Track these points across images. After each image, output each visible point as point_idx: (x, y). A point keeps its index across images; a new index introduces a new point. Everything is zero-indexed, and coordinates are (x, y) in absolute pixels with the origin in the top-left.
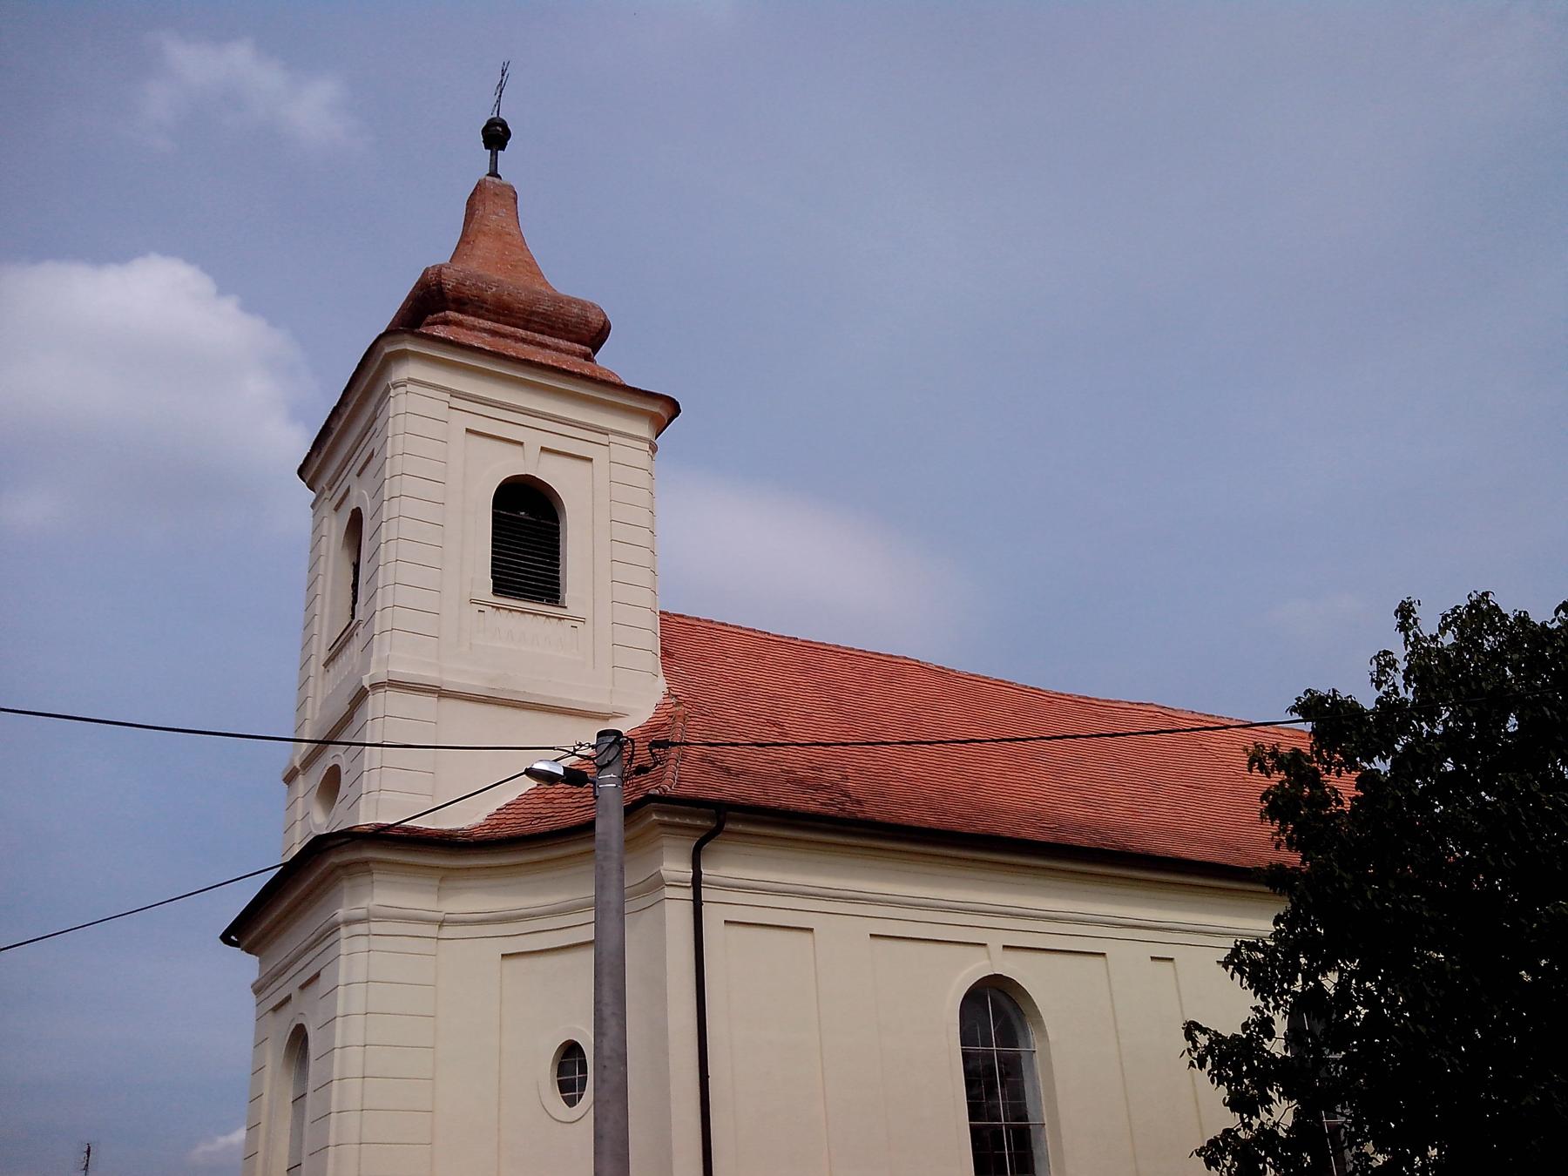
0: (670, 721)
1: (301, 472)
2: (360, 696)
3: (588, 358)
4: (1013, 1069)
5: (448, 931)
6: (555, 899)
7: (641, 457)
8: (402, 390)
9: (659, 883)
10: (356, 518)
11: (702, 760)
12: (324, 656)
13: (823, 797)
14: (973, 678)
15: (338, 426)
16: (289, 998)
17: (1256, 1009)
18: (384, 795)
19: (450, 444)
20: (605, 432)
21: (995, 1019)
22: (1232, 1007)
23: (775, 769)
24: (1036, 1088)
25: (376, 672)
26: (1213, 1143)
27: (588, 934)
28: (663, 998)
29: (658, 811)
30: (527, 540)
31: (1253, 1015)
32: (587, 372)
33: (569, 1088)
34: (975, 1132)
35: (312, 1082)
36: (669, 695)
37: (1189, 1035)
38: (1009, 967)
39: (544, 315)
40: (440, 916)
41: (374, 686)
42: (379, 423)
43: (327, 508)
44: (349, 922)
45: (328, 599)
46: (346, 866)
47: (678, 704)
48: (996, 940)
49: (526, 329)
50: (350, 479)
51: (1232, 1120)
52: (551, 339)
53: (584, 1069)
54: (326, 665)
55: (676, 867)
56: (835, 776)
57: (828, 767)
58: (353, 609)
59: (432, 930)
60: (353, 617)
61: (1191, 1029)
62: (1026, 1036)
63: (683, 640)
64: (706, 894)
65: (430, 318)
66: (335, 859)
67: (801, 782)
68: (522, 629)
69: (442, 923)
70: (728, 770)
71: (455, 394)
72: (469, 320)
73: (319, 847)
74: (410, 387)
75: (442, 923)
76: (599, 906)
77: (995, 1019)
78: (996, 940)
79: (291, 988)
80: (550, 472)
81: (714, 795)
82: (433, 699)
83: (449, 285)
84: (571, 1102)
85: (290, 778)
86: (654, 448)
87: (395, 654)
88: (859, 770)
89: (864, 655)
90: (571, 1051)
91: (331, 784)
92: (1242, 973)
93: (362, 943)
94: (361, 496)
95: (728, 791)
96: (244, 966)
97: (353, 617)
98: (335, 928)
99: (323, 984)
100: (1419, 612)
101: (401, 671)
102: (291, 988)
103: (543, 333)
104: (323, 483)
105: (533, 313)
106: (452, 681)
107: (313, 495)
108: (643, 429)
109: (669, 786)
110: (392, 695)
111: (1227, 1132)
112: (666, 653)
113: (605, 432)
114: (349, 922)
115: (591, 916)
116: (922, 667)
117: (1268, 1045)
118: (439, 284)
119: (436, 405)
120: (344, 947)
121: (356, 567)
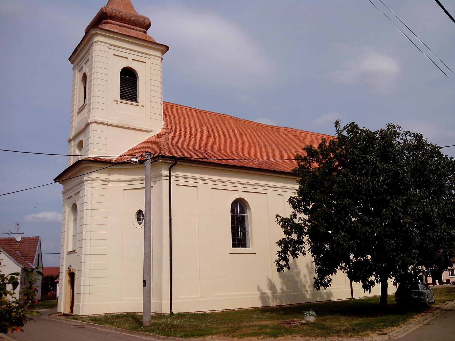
0: (165, 133)
1: (69, 59)
2: (88, 125)
3: (145, 33)
4: (243, 219)
5: (111, 183)
6: (135, 178)
7: (158, 62)
8: (96, 43)
9: (161, 176)
10: (85, 76)
11: (173, 145)
12: (77, 111)
13: (201, 156)
14: (244, 121)
15: (79, 49)
16: (72, 196)
17: (293, 212)
18: (94, 150)
19: (109, 58)
20: (149, 55)
21: (239, 210)
22: (287, 211)
23: (191, 147)
24: (248, 224)
25: (91, 119)
26: (280, 241)
27: (144, 186)
28: (161, 202)
29: (161, 159)
30: (129, 83)
31: (292, 213)
32: (144, 38)
33: (139, 220)
34: (233, 233)
35: (78, 217)
36: (165, 126)
37: (276, 217)
38: (244, 196)
39: (133, 21)
40: (109, 180)
41: (91, 123)
42: (91, 51)
43: (76, 71)
44: (86, 181)
45: (78, 95)
46: (86, 167)
47: (167, 129)
48: (241, 190)
49: (129, 24)
50: (83, 64)
51: (285, 236)
52: (136, 28)
53: (143, 216)
54: (78, 113)
55: (165, 172)
56: (205, 149)
57: (204, 147)
58: (85, 101)
59: (107, 183)
60: (85, 102)
61: (277, 216)
62: (247, 211)
63: (169, 110)
64: (172, 178)
65: (103, 21)
66: (83, 166)
67: (197, 151)
68: (127, 107)
69: (109, 181)
70: (178, 148)
71: (110, 45)
72: (114, 22)
73: (78, 163)
74: (99, 43)
75: (109, 181)
76: (146, 179)
77: (239, 210)
78: (241, 190)
79: (72, 194)
80: (135, 66)
81: (175, 155)
82: (106, 126)
83: (108, 13)
84: (140, 223)
85: (70, 141)
86: (162, 59)
87: (96, 116)
88: (212, 148)
89: (217, 114)
90: (140, 212)
91: (80, 145)
92: (291, 203)
93: (90, 185)
94: (86, 69)
95: (178, 154)
96: (59, 187)
97: (85, 102)
98: (83, 182)
99: (81, 194)
100: (340, 123)
101: (98, 119)
102: (72, 194)
103: (133, 25)
104: (76, 63)
105: (130, 20)
106: (110, 122)
107: (72, 66)
108: (159, 54)
109: (164, 153)
110: (96, 125)
111: (283, 239)
112: (164, 114)
113: (149, 55)
114: (86, 181)
115: (144, 182)
116: (231, 118)
117: (294, 220)
118: (106, 12)
119: (105, 48)
120: (86, 186)
121: (85, 88)
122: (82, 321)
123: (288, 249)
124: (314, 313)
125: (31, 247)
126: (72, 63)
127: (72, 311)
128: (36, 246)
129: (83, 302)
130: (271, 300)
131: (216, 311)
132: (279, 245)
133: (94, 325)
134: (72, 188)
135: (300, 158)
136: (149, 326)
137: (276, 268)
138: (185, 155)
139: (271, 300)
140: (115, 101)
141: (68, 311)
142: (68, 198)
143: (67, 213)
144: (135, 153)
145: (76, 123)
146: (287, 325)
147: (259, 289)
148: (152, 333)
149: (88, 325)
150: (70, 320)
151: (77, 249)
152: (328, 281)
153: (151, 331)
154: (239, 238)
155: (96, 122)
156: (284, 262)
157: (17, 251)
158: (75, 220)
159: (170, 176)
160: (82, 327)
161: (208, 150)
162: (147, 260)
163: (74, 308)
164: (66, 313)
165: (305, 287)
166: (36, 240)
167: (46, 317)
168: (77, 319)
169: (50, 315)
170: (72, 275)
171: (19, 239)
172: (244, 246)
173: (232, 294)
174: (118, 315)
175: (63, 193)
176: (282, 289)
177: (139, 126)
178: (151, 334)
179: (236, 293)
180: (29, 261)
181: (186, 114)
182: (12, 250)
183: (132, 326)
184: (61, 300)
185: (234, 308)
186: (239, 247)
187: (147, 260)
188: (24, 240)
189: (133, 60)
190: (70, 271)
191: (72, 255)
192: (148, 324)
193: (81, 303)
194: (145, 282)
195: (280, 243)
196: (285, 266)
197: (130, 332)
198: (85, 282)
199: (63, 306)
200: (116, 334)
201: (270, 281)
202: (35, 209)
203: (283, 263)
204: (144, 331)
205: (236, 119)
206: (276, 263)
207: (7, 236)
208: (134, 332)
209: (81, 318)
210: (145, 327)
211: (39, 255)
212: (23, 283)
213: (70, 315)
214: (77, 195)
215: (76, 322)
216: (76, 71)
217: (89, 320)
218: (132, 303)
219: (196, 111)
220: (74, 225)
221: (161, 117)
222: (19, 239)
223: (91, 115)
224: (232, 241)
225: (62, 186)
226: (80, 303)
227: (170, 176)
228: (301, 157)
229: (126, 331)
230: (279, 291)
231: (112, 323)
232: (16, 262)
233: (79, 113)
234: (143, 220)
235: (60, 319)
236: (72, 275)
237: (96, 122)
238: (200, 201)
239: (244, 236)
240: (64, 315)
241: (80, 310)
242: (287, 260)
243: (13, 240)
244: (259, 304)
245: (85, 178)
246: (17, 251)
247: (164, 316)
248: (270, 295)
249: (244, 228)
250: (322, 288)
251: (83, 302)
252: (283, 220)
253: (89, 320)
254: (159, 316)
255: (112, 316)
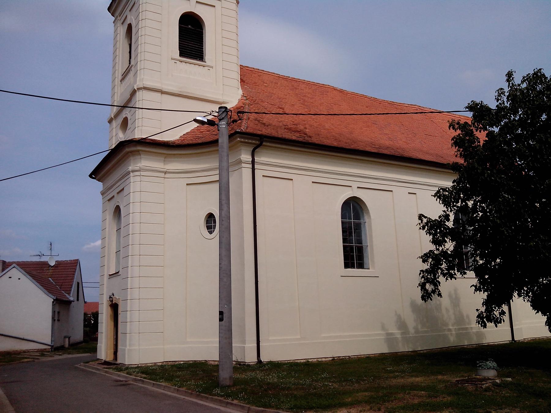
0: (243, 106)
4: (358, 228)
5: (167, 175)
6: (205, 166)
9: (240, 162)
10: (130, 27)
11: (255, 120)
12: (120, 77)
14: (353, 94)
16: (113, 197)
17: (444, 211)
18: (143, 128)
21: (353, 211)
22: (436, 210)
23: (281, 124)
24: (366, 234)
29: (240, 137)
31: (443, 213)
34: (344, 247)
38: (359, 194)
40: (165, 170)
41: (139, 89)
43: (119, 23)
44: (133, 171)
46: (131, 152)
47: (246, 100)
48: (355, 185)
51: (433, 247)
53: (215, 222)
55: (246, 157)
58: (130, 61)
59: (162, 175)
60: (130, 63)
61: (421, 217)
62: (363, 217)
63: (248, 76)
64: (256, 166)
66: (127, 150)
67: (290, 129)
68: (189, 69)
69: (165, 173)
70: (264, 124)
73: (122, 145)
75: (165, 173)
76: (220, 169)
77: (353, 211)
78: (355, 185)
79: (114, 193)
80: (200, 11)
81: (259, 133)
82: (159, 94)
84: (211, 233)
85: (110, 121)
87: (145, 78)
88: (311, 126)
91: (125, 124)
93: (138, 178)
94: (131, 19)
95: (265, 131)
96: (98, 186)
97: (130, 63)
98: (129, 173)
99: (125, 192)
100: (515, 75)
101: (149, 83)
102: (114, 193)
104: (117, 14)
106: (166, 88)
107: (113, 18)
110: (145, 92)
112: (242, 81)
114: (133, 171)
115: (217, 172)
116: (335, 89)
120: (132, 179)
122: (127, 374)
123: (437, 267)
124: (494, 364)
125: (68, 273)
126: (113, 15)
127: (116, 358)
128: (75, 272)
129: (130, 345)
130: (400, 345)
131: (324, 360)
132: (424, 261)
133: (143, 381)
134: (114, 185)
135: (457, 126)
136: (229, 386)
137: (419, 293)
138: (274, 133)
139: (400, 345)
140: (172, 59)
141: (110, 358)
142: (109, 200)
143: (107, 220)
144: (202, 132)
145: (119, 95)
146: (470, 387)
147: (383, 328)
148: (236, 399)
149: (135, 380)
150: (111, 371)
151: (121, 270)
152: (500, 314)
153: (234, 396)
154: (354, 255)
155: (145, 88)
156: (433, 287)
157: (50, 279)
158: (119, 230)
159: (253, 162)
160: (125, 384)
161: (306, 128)
162: (225, 280)
163: (119, 353)
164: (108, 360)
165: (447, 325)
166: (75, 264)
167: (81, 366)
168: (120, 370)
169: (87, 363)
170: (114, 307)
171: (52, 263)
172: (361, 266)
173: (345, 334)
174: (180, 364)
175: (103, 194)
176: (416, 329)
177: (207, 95)
178: (235, 402)
179: (351, 334)
180: (65, 291)
181: (272, 82)
182: (43, 276)
183: (201, 385)
184: (102, 343)
185: (350, 355)
186: (354, 268)
187: (225, 280)
188: (59, 264)
189: (197, 2)
190: (112, 301)
191: (115, 279)
192: (228, 383)
193: (128, 347)
194: (221, 313)
195: (425, 258)
196: (434, 292)
197: (198, 396)
198: (131, 316)
199: (104, 351)
200: (175, 398)
201: (399, 317)
202: (60, 214)
203: (429, 287)
204: (222, 396)
205: (341, 91)
206: (420, 287)
207: (37, 259)
208: (205, 397)
209: (127, 368)
210: (223, 387)
211: (78, 283)
212: (56, 318)
213: (113, 364)
214: (121, 194)
215: (119, 376)
216: (119, 23)
217: (138, 373)
218: (203, 347)
219: (286, 79)
220: (117, 235)
221: (238, 84)
222: (52, 263)
223: (138, 79)
224: (345, 260)
225: (100, 184)
226: (126, 346)
227: (253, 162)
228: (458, 123)
229: (192, 394)
230: (412, 330)
231: (169, 379)
232: (46, 291)
233: (122, 80)
234: (215, 228)
235: (98, 369)
236: (114, 307)
237: (145, 88)
238: (298, 200)
239: (360, 251)
240: (106, 363)
241: (126, 356)
242: (436, 284)
243: (45, 265)
244: (385, 350)
245: (130, 168)
246: (50, 279)
247: (249, 366)
248: (399, 336)
249: (360, 241)
250: (490, 325)
251: (130, 345)
252: (430, 221)
253: (138, 373)
254: (241, 367)
255: (172, 366)
